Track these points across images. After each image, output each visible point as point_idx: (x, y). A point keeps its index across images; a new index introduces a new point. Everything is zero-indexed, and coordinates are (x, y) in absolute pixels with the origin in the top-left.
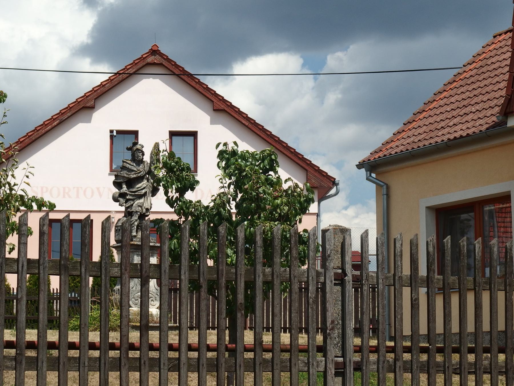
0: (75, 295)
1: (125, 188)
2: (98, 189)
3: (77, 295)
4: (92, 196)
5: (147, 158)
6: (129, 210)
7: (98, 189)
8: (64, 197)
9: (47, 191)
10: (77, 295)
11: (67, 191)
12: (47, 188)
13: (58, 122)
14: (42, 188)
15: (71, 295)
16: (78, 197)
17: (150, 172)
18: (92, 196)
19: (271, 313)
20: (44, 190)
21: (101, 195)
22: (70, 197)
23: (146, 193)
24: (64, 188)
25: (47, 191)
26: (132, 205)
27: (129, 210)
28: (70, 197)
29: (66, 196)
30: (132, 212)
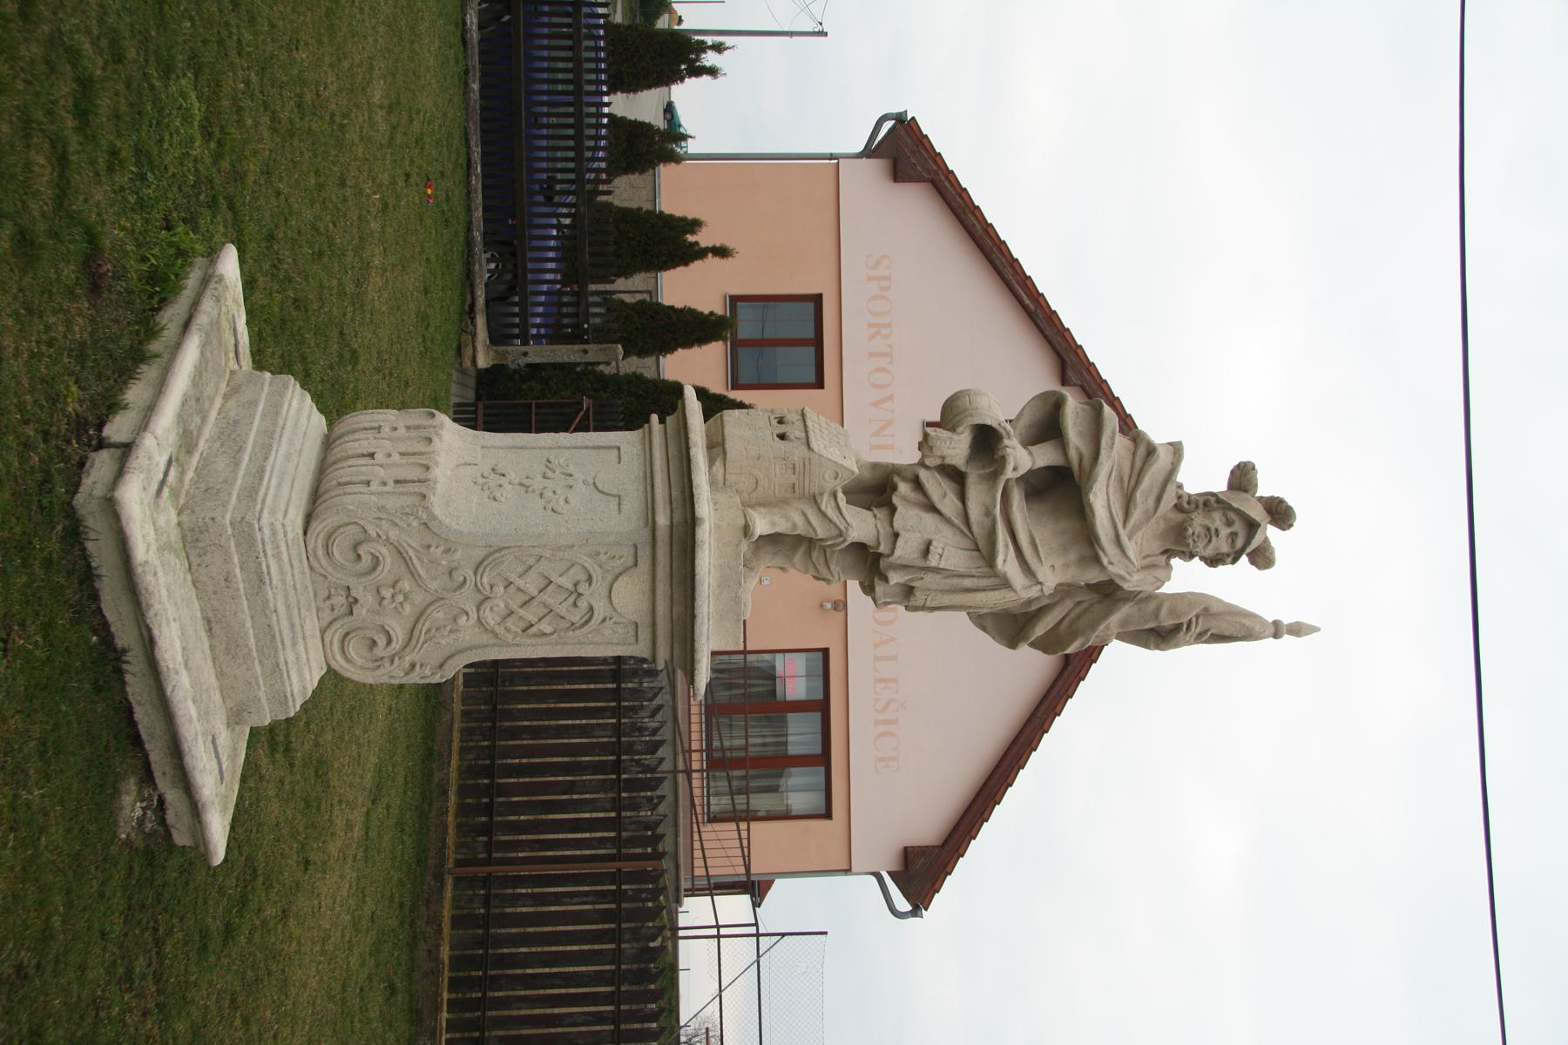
0: (596, 315)
1: (1021, 459)
2: (890, 398)
3: (597, 320)
4: (875, 386)
5: (1188, 577)
6: (904, 488)
7: (890, 398)
8: (871, 325)
9: (881, 288)
10: (597, 320)
11: (884, 331)
12: (888, 288)
13: (1032, 307)
14: (888, 278)
15: (596, 304)
16: (872, 355)
17: (1108, 593)
18: (875, 386)
19: (578, 853)
20: (884, 283)
21: (876, 404)
22: (871, 338)
23: (1005, 584)
24: (889, 325)
25: (881, 288)
26: (932, 508)
27: (904, 488)
28: (871, 338)
29: (873, 330)
30: (893, 510)
